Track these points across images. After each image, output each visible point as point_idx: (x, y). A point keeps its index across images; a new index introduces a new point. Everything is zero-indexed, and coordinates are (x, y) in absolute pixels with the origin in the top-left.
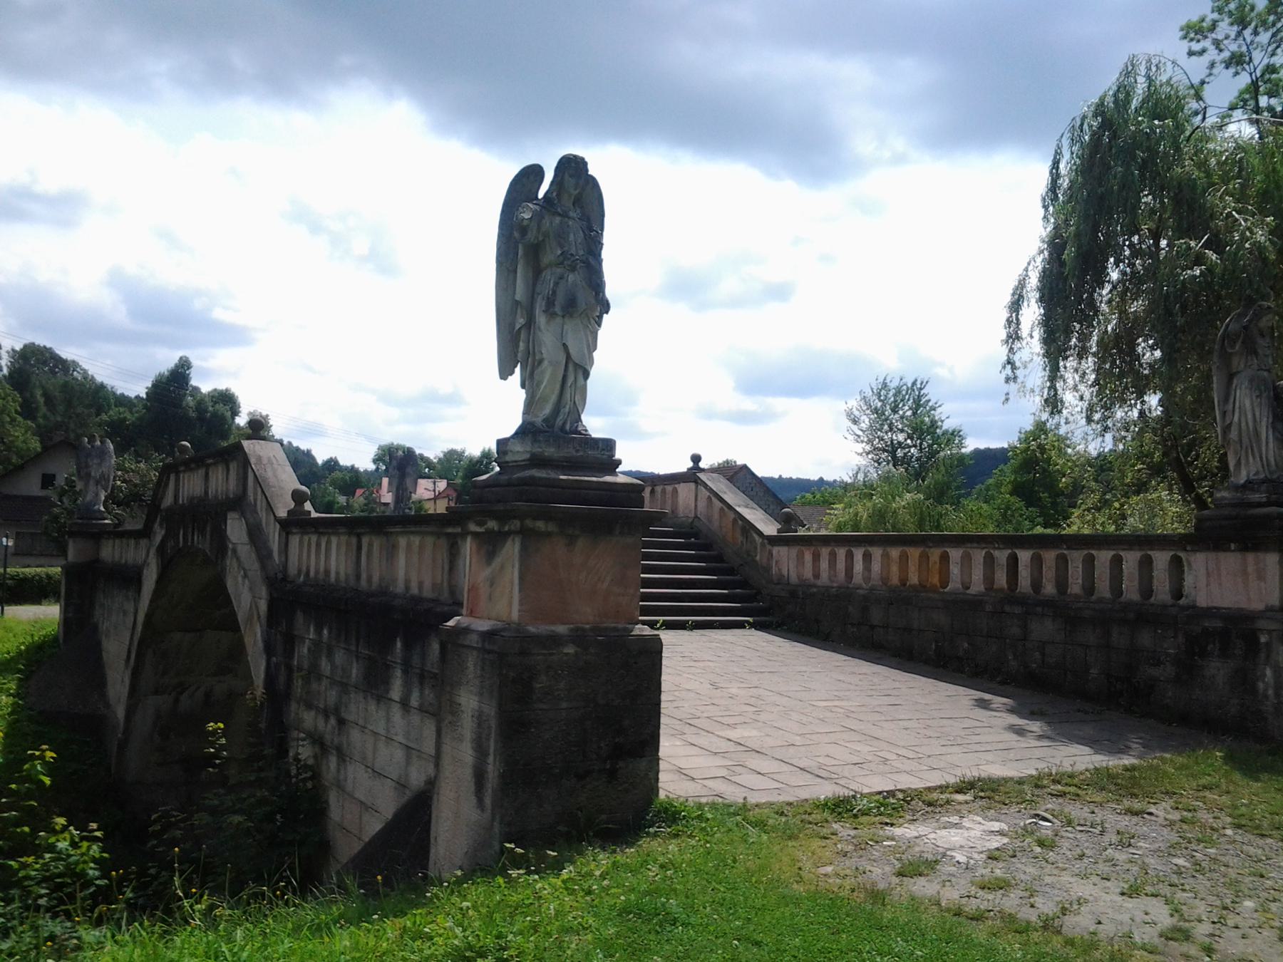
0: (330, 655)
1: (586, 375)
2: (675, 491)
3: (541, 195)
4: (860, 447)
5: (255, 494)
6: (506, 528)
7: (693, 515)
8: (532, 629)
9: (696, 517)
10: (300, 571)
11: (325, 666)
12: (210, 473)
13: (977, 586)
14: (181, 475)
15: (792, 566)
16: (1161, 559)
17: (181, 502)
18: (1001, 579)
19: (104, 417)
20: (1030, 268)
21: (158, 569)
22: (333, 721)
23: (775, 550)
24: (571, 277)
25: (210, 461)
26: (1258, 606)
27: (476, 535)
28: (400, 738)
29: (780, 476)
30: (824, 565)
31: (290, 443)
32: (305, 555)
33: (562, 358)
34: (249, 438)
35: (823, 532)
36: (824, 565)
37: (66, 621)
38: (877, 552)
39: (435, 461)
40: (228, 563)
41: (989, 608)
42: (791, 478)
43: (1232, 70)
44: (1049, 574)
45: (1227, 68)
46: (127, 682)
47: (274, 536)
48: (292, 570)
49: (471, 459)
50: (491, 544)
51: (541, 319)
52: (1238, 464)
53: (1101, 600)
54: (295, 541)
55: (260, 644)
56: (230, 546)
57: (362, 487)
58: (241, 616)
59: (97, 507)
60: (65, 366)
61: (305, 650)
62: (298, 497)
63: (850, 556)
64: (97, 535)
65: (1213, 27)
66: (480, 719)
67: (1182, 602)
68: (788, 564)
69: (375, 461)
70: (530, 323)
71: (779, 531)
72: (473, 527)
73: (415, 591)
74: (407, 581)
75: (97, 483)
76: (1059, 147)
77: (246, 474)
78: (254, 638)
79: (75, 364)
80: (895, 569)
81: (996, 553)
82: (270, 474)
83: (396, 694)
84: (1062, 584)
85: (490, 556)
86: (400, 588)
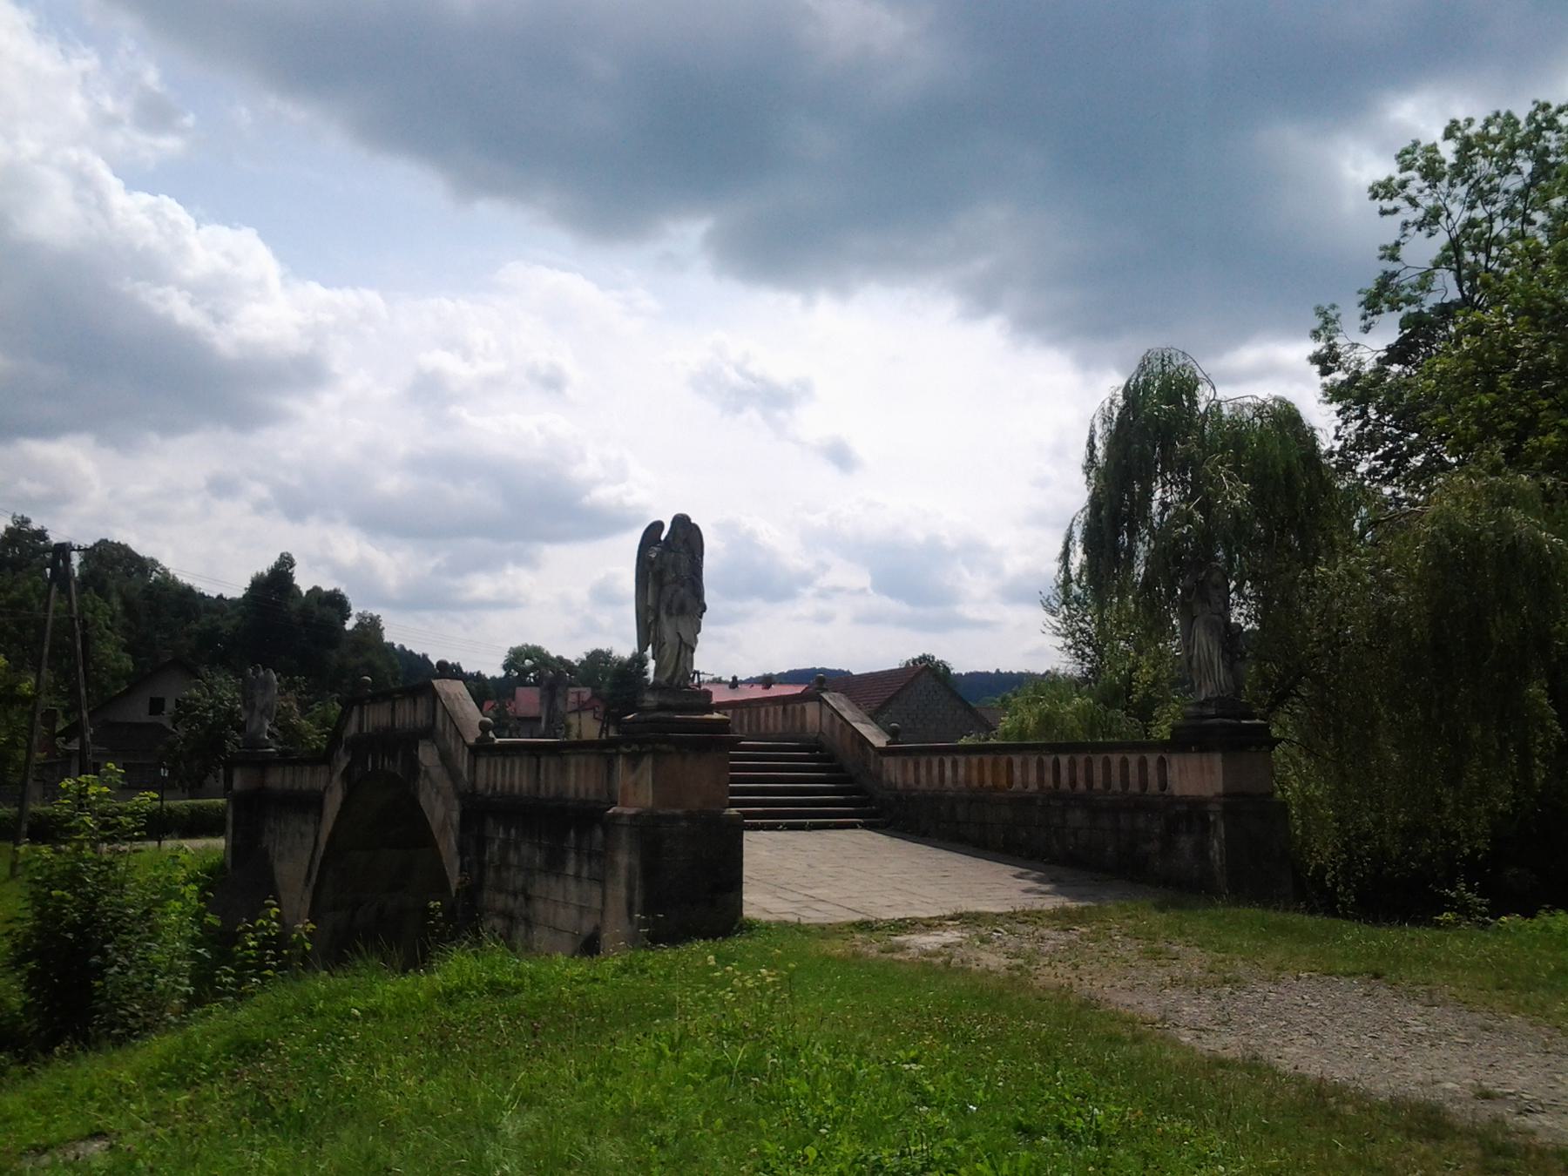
0: (517, 849)
1: (693, 650)
2: (803, 710)
3: (663, 538)
4: (1060, 641)
5: (444, 725)
6: (644, 750)
7: (817, 731)
8: (660, 812)
9: (821, 732)
10: (487, 785)
11: (513, 857)
12: (397, 706)
13: (1033, 786)
14: (366, 707)
15: (898, 776)
16: (1152, 759)
17: (365, 731)
18: (1049, 779)
19: (194, 626)
20: (1075, 523)
21: (344, 790)
22: (521, 898)
23: (886, 760)
24: (682, 591)
25: (397, 696)
26: (1209, 793)
27: (625, 755)
28: (574, 901)
29: (998, 670)
30: (923, 771)
31: (402, 647)
32: (492, 773)
33: (678, 640)
34: (437, 677)
35: (992, 741)
36: (923, 771)
37: (235, 849)
38: (961, 759)
39: (576, 664)
40: (421, 782)
41: (1039, 803)
42: (1011, 673)
43: (1425, 231)
44: (1080, 773)
45: (1419, 229)
46: (308, 898)
47: (463, 764)
48: (481, 785)
49: (621, 663)
50: (634, 760)
51: (663, 616)
52: (1200, 685)
53: (1115, 793)
54: (482, 764)
55: (455, 849)
56: (423, 768)
57: (490, 699)
58: (434, 827)
59: (261, 736)
60: (142, 565)
61: (496, 847)
62: (484, 727)
63: (942, 764)
64: (264, 764)
65: (1403, 185)
66: (630, 869)
67: (1166, 792)
68: (895, 772)
69: (505, 667)
70: (657, 618)
71: (888, 743)
72: (624, 750)
73: (582, 796)
74: (577, 791)
75: (262, 712)
76: (1093, 426)
77: (435, 709)
78: (448, 845)
79: (154, 562)
80: (975, 773)
81: (1045, 758)
82: (457, 707)
83: (571, 869)
84: (1089, 782)
85: (634, 767)
86: (571, 794)
